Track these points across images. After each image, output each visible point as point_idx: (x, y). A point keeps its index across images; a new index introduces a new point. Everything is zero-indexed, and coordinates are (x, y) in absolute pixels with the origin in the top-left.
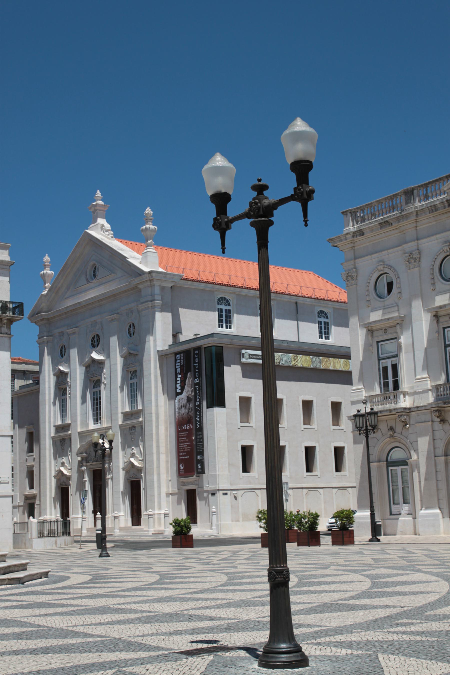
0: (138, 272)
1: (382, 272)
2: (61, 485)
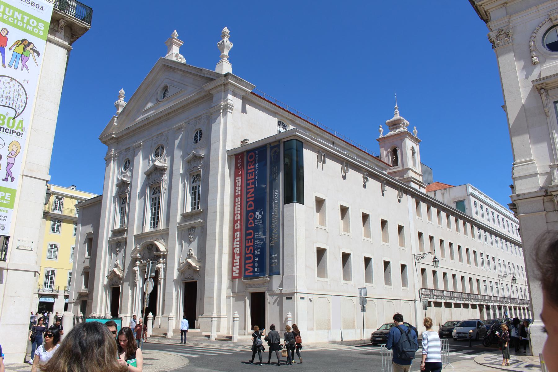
2: (113, 284)
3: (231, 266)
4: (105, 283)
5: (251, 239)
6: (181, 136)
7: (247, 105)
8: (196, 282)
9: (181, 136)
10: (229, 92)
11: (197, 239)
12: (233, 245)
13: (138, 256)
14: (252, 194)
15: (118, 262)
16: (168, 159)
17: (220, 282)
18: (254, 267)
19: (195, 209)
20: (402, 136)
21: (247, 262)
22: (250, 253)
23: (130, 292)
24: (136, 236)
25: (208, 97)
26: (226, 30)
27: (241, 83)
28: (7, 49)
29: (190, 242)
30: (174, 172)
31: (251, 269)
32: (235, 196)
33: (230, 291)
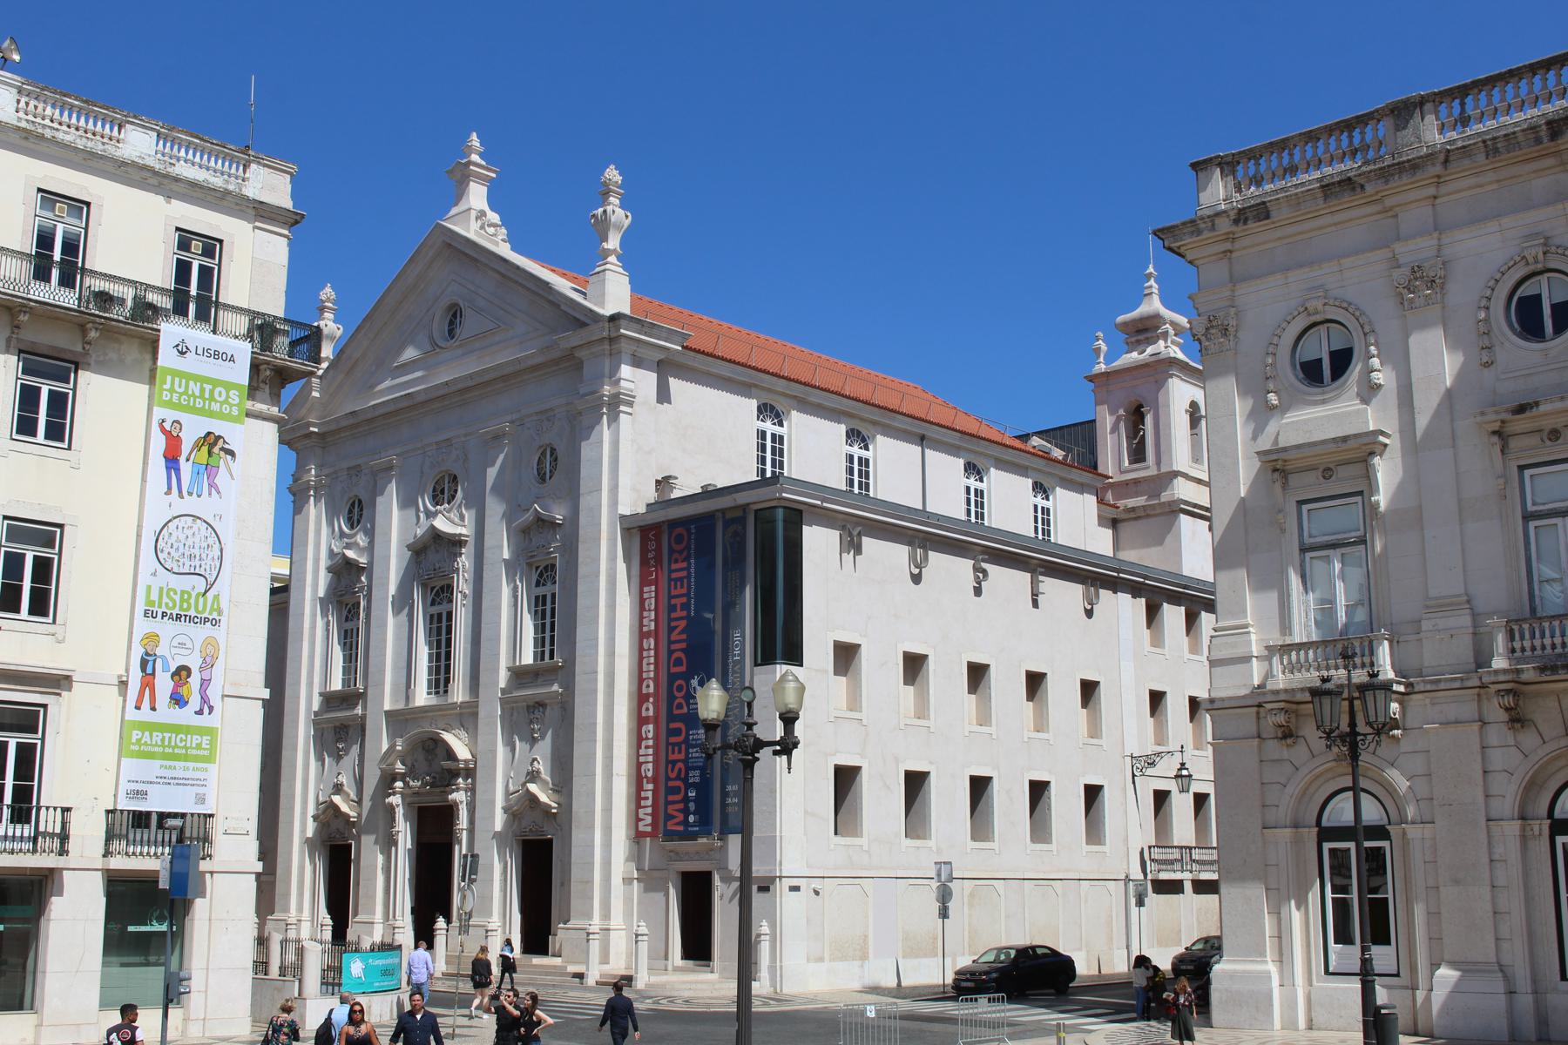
0: (580, 319)
1: (1318, 318)
3: (633, 807)
4: (310, 834)
5: (679, 744)
6: (501, 457)
7: (671, 380)
8: (551, 841)
9: (501, 457)
10: (624, 357)
11: (550, 733)
12: (638, 755)
13: (400, 767)
14: (683, 631)
15: (343, 779)
16: (469, 516)
17: (607, 845)
18: (686, 812)
19: (543, 659)
20: (1162, 368)
21: (671, 798)
22: (678, 778)
23: (380, 859)
24: (389, 714)
25: (570, 363)
26: (613, 174)
27: (655, 331)
28: (182, 459)
29: (533, 741)
30: (487, 554)
31: (681, 817)
32: (643, 636)
33: (633, 865)
